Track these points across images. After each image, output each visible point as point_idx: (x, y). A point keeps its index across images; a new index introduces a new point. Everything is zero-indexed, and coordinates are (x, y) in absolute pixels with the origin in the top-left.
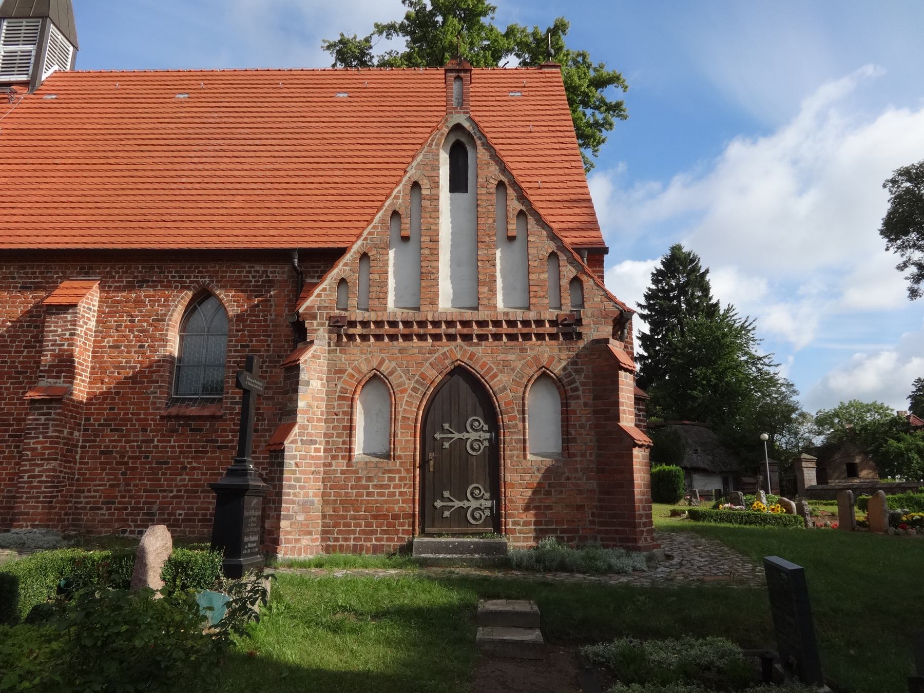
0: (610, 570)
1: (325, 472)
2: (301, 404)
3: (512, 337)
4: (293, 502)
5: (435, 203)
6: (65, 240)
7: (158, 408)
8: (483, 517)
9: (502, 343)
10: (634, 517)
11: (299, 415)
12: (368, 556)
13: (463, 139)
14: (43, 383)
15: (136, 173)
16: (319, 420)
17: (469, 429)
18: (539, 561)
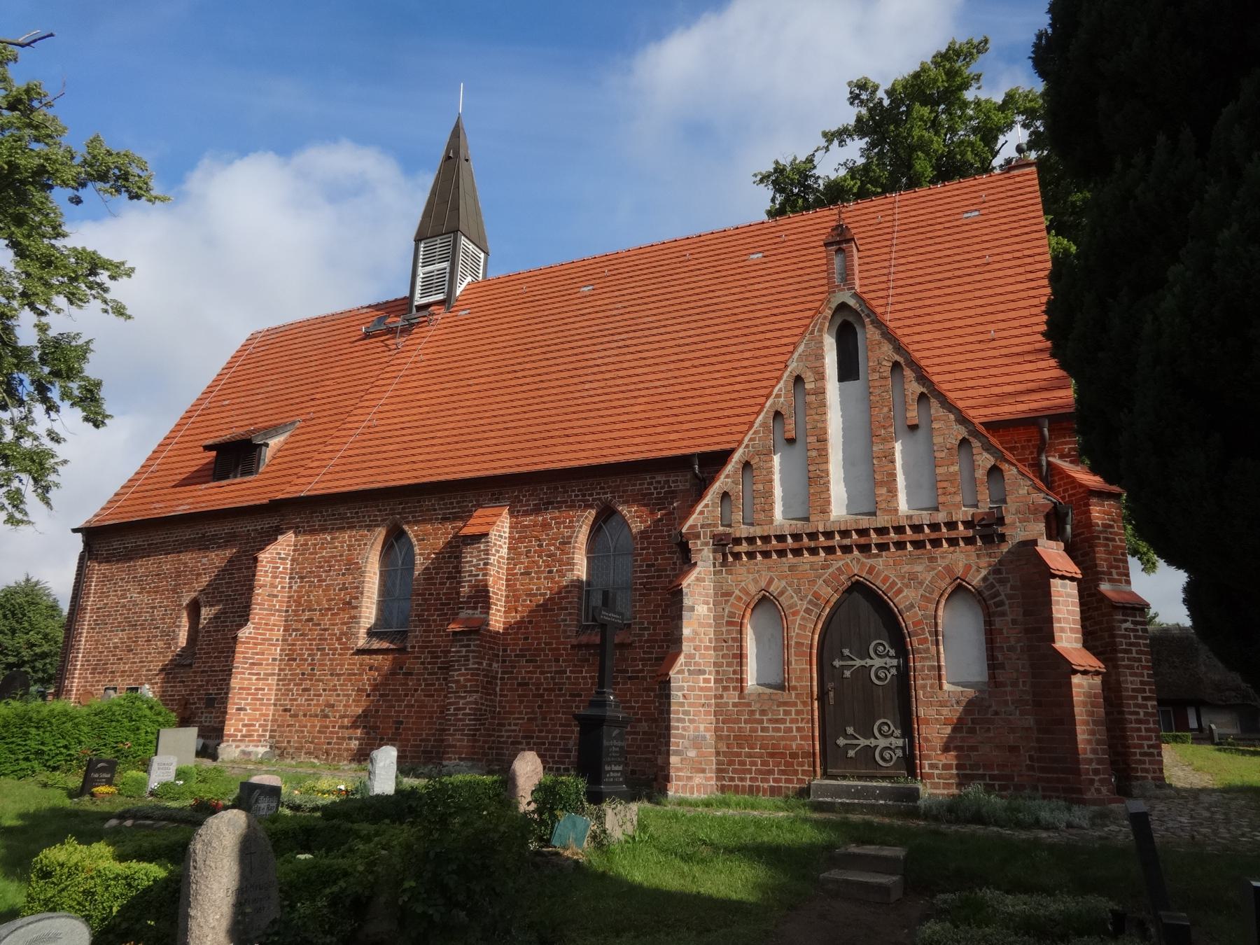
0: (1037, 824)
1: (717, 705)
2: (686, 632)
4: (683, 737)
5: (821, 397)
6: (477, 467)
7: (569, 637)
8: (894, 758)
9: (906, 552)
10: (1077, 761)
11: (684, 644)
12: (763, 799)
13: (851, 319)
14: (464, 614)
16: (707, 648)
17: (872, 654)
18: (953, 810)
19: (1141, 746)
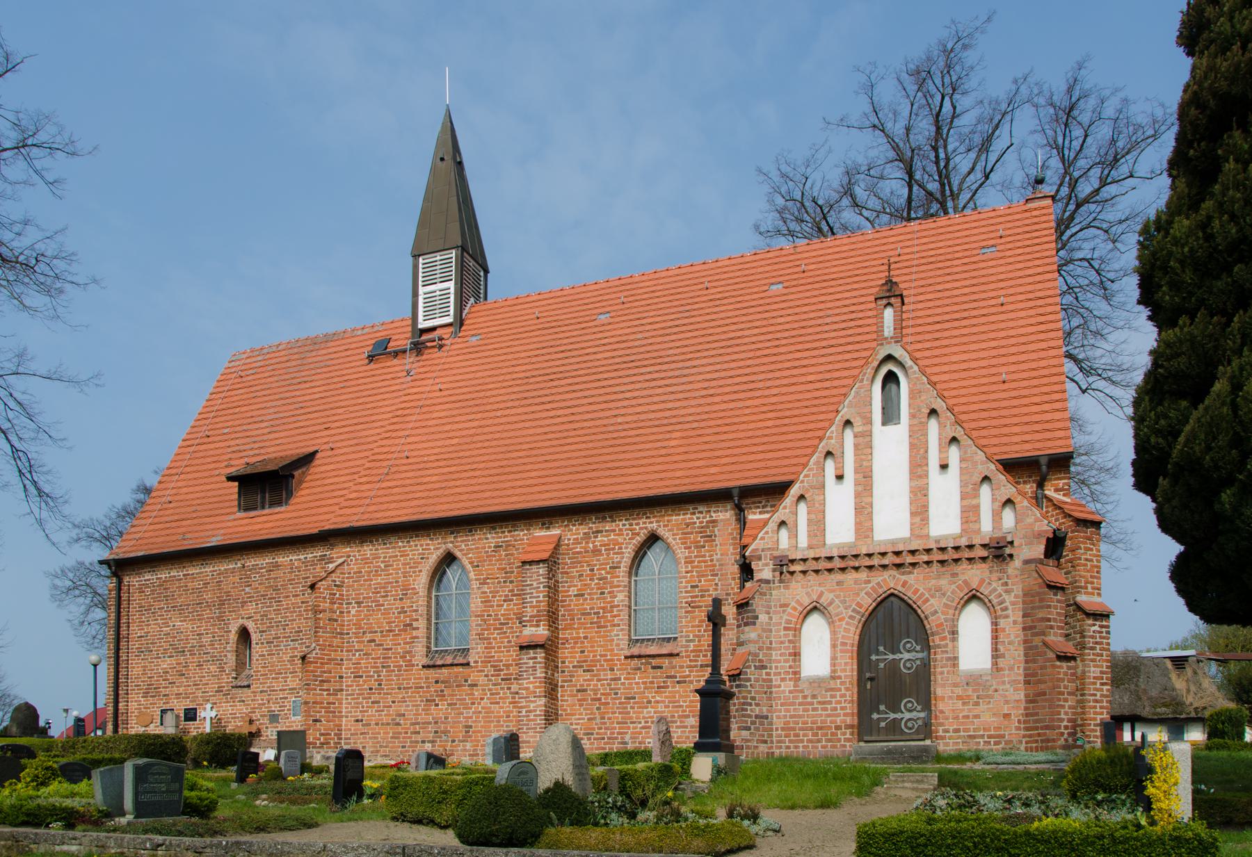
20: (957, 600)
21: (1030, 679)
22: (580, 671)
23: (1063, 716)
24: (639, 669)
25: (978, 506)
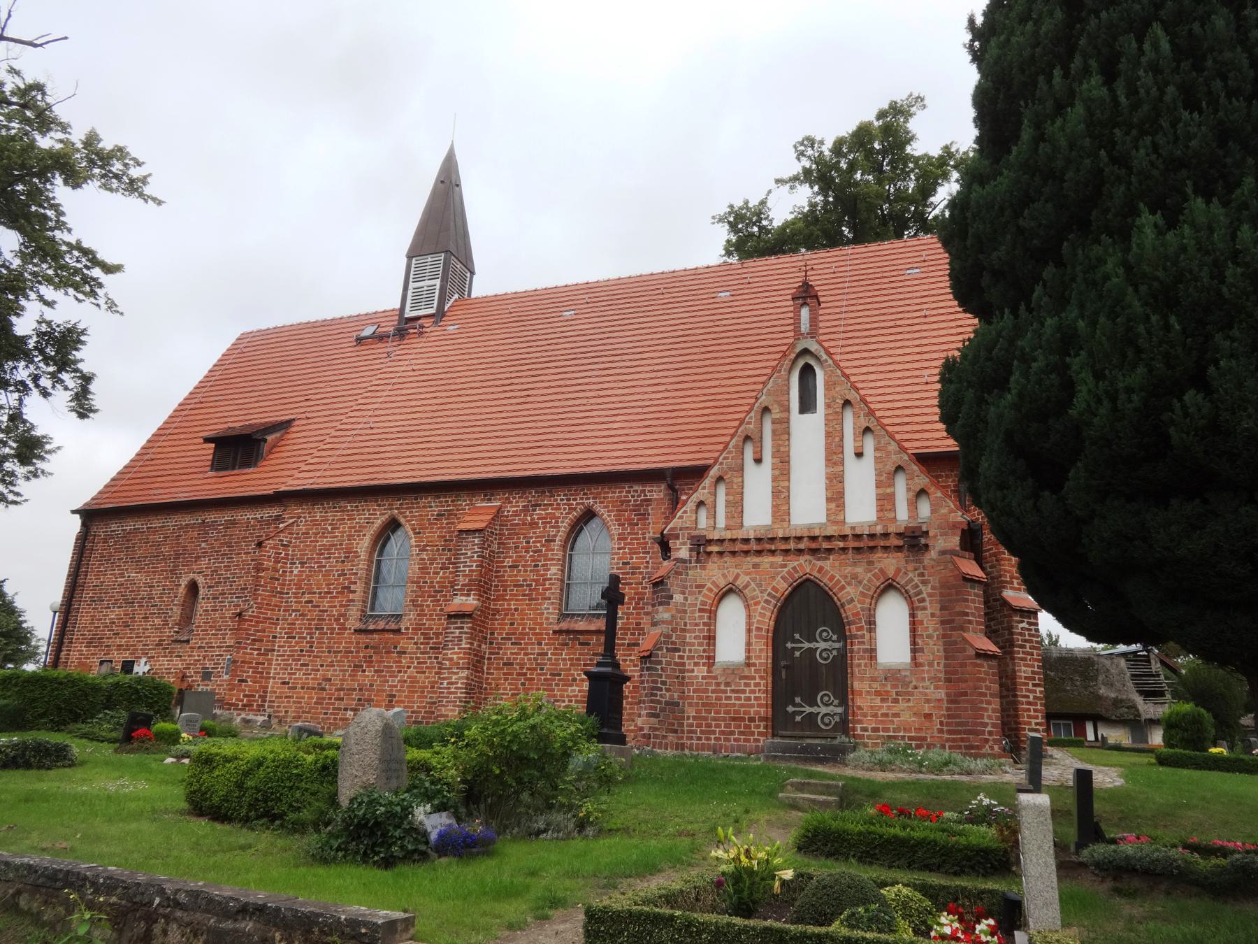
3: (858, 550)
13: (812, 362)
15: (529, 399)
19: (1030, 723)
20: (873, 589)
21: (951, 678)
22: (509, 644)
23: (986, 720)
24: (567, 644)
25: (893, 494)
